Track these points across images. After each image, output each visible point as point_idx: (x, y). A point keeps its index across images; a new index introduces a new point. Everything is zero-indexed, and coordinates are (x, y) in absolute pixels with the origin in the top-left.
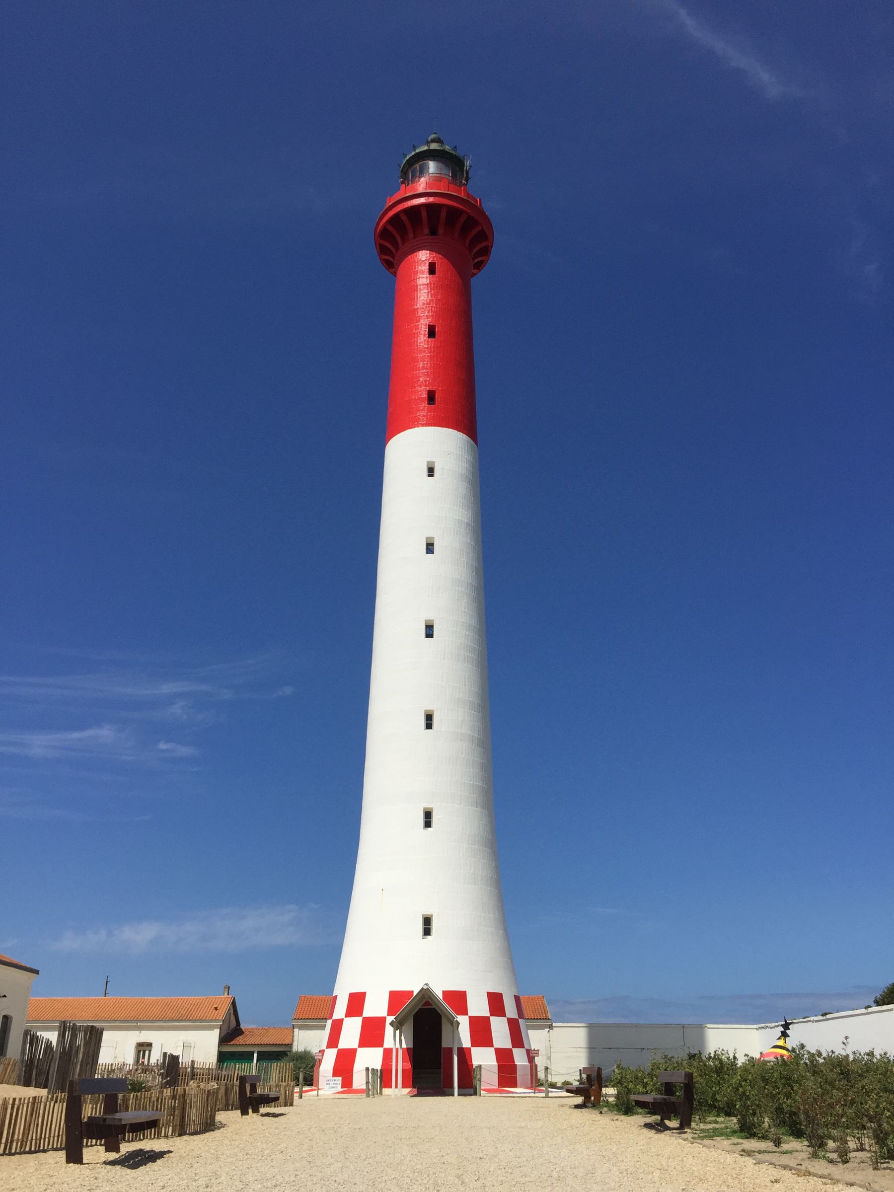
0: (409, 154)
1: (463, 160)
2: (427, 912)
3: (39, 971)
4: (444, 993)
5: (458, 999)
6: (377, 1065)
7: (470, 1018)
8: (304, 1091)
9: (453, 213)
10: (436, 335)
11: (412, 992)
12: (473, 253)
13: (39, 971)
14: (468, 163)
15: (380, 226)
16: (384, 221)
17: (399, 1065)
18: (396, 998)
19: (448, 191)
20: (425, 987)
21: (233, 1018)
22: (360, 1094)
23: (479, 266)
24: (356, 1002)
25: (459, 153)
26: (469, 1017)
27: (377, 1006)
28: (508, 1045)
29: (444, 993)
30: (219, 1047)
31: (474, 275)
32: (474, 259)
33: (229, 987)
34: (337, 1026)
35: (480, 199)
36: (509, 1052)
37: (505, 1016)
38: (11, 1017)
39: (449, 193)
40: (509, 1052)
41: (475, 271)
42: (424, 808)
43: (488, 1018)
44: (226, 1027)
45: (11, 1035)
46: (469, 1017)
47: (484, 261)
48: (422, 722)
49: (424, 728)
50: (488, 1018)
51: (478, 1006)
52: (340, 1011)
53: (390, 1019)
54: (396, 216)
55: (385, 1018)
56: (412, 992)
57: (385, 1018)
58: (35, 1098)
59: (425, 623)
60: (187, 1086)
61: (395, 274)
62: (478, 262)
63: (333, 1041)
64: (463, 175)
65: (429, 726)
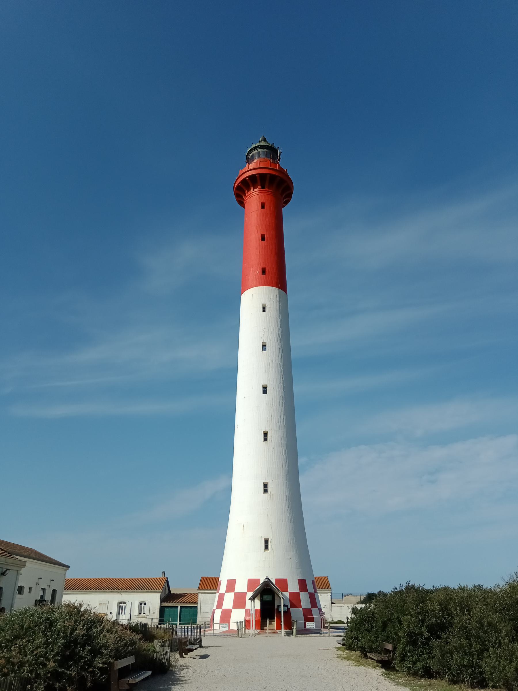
1: (277, 149)
2: (267, 537)
3: (69, 566)
4: (276, 580)
5: (283, 583)
7: (289, 592)
9: (272, 177)
10: (265, 239)
11: (259, 579)
12: (283, 197)
13: (69, 566)
14: (279, 151)
16: (237, 182)
17: (253, 619)
18: (251, 583)
19: (270, 167)
20: (267, 580)
21: (167, 588)
23: (286, 203)
24: (231, 585)
25: (276, 146)
27: (241, 587)
29: (276, 580)
30: (160, 604)
31: (284, 206)
32: (283, 200)
33: (165, 572)
34: (221, 598)
35: (286, 170)
39: (271, 167)
42: (264, 482)
43: (299, 593)
44: (163, 594)
47: (288, 200)
48: (261, 309)
49: (263, 441)
50: (299, 593)
51: (293, 587)
52: (223, 588)
53: (250, 595)
54: (244, 180)
56: (259, 579)
59: (262, 344)
61: (244, 207)
63: (220, 605)
64: (278, 158)
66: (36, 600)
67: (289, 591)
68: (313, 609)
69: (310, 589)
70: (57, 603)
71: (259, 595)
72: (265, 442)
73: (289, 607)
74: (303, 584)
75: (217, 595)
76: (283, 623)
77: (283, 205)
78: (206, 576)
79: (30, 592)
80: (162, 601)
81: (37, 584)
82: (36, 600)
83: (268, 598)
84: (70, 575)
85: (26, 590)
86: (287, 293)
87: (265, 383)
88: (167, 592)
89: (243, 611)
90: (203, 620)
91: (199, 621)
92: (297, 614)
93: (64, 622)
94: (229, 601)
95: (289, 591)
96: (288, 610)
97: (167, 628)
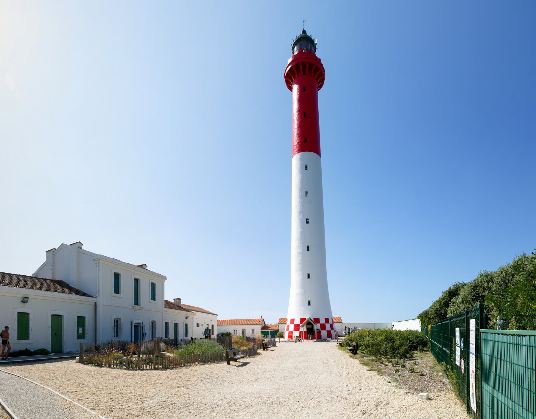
0: (293, 137)
2: (309, 300)
4: (314, 319)
6: (298, 335)
7: (319, 323)
8: (461, 339)
12: (316, 77)
15: (286, 74)
16: (287, 71)
22: (467, 391)
24: (292, 321)
26: (320, 324)
27: (297, 322)
28: (324, 323)
29: (314, 319)
31: (319, 90)
32: (318, 84)
34: (288, 326)
36: (330, 331)
37: (329, 323)
38: (178, 323)
40: (330, 331)
41: (319, 88)
45: (169, 327)
46: (320, 324)
48: (306, 249)
51: (322, 321)
52: (289, 322)
55: (299, 325)
57: (299, 325)
58: (500, 329)
60: (143, 340)
61: (292, 91)
62: (320, 85)
63: (288, 329)
65: (308, 250)
66: (205, 329)
67: (320, 323)
68: (332, 331)
69: (331, 322)
70: (294, 337)
71: (306, 325)
72: (308, 251)
73: (320, 330)
74: (327, 320)
75: (286, 326)
76: (316, 337)
77: (319, 88)
78: (296, 140)
79: (202, 326)
80: (262, 329)
81: (205, 322)
82: (205, 329)
83: (310, 326)
84: (219, 318)
85: (200, 325)
86: (320, 157)
87: (307, 217)
88: (264, 325)
89: (298, 332)
90: (389, 328)
91: (533, 348)
92: (324, 333)
93: (522, 327)
94: (292, 328)
95: (320, 323)
96: (320, 332)
97: (147, 366)
